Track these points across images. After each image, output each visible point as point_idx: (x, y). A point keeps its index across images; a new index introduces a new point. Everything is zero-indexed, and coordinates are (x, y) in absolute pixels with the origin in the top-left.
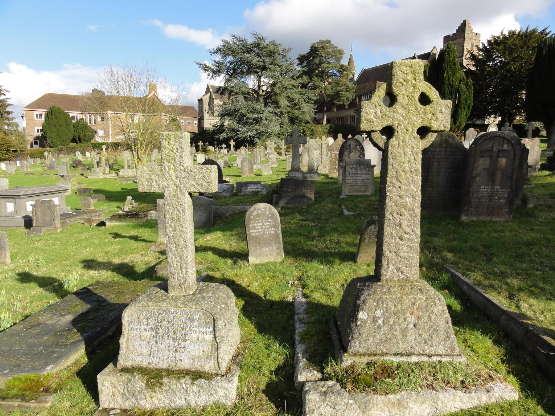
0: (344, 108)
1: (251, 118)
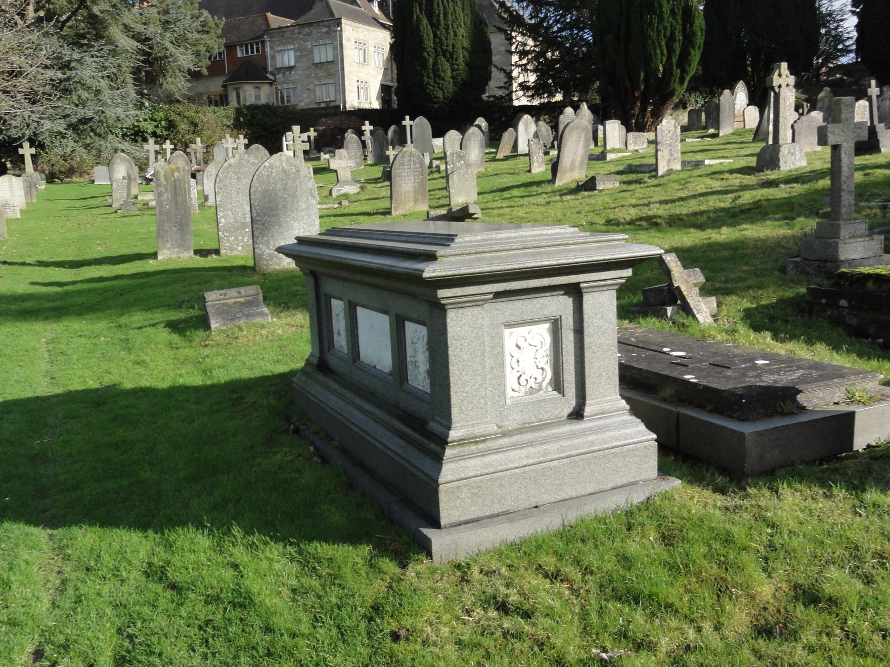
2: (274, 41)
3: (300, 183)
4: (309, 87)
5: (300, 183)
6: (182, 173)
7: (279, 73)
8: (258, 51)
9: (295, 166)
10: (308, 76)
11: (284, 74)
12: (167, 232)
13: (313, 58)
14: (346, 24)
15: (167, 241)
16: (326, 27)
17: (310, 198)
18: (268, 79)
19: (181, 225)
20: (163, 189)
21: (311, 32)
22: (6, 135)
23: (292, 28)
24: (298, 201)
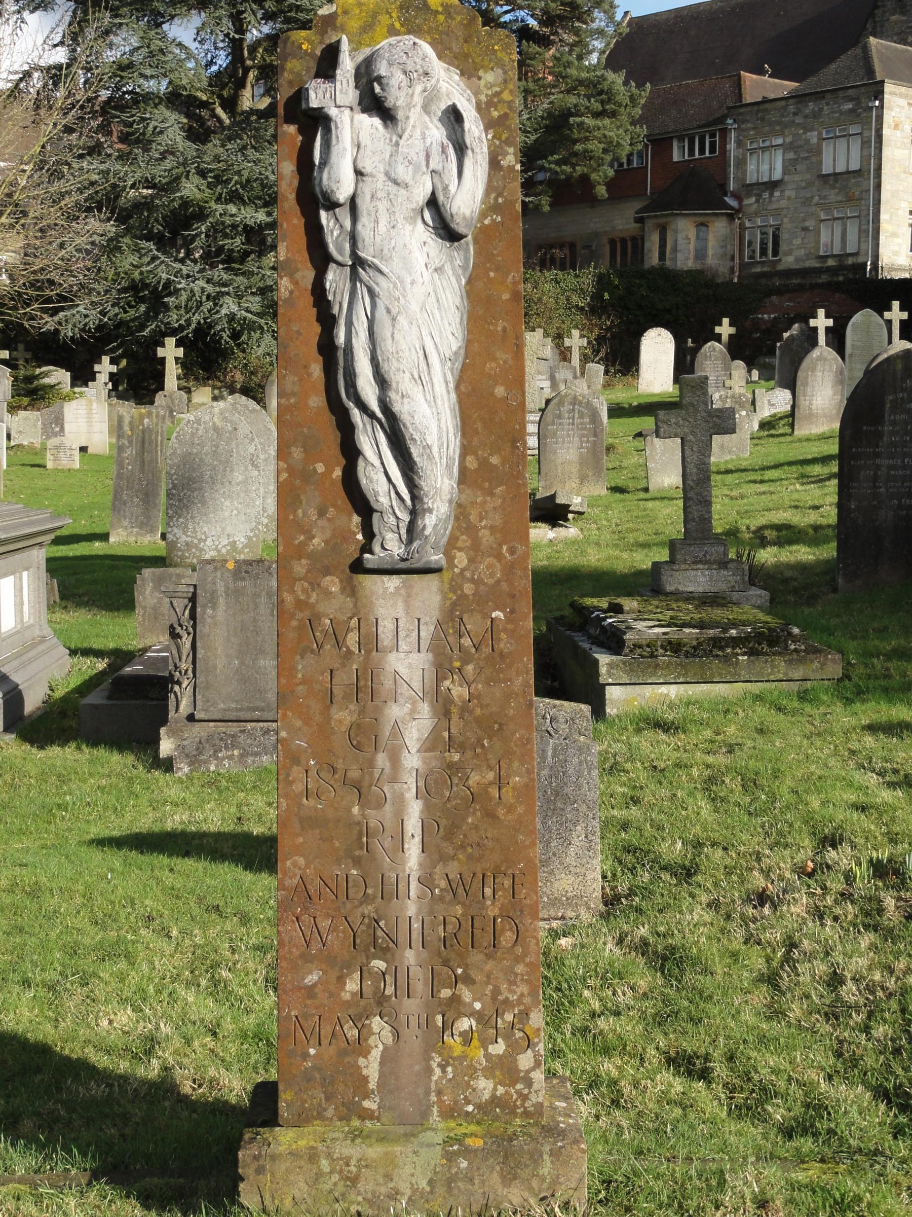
0: (593, 201)
1: (234, 226)
2: (744, 130)
3: (237, 445)
4: (807, 224)
5: (237, 445)
6: (155, 420)
7: (749, 195)
8: (712, 150)
9: (231, 422)
10: (807, 202)
11: (759, 196)
12: (125, 503)
13: (820, 163)
14: (891, 93)
15: (125, 517)
16: (851, 99)
17: (250, 467)
18: (727, 206)
19: (147, 495)
20: (126, 442)
21: (821, 110)
22: (162, 322)
23: (783, 103)
24: (232, 471)
